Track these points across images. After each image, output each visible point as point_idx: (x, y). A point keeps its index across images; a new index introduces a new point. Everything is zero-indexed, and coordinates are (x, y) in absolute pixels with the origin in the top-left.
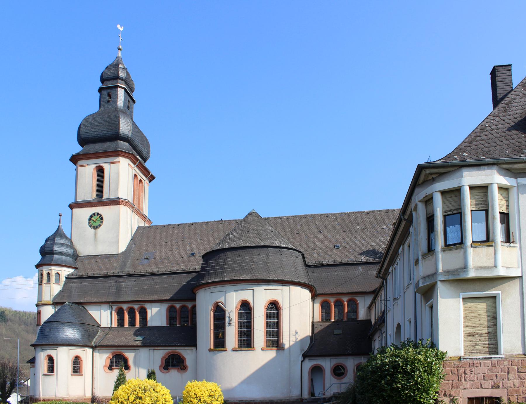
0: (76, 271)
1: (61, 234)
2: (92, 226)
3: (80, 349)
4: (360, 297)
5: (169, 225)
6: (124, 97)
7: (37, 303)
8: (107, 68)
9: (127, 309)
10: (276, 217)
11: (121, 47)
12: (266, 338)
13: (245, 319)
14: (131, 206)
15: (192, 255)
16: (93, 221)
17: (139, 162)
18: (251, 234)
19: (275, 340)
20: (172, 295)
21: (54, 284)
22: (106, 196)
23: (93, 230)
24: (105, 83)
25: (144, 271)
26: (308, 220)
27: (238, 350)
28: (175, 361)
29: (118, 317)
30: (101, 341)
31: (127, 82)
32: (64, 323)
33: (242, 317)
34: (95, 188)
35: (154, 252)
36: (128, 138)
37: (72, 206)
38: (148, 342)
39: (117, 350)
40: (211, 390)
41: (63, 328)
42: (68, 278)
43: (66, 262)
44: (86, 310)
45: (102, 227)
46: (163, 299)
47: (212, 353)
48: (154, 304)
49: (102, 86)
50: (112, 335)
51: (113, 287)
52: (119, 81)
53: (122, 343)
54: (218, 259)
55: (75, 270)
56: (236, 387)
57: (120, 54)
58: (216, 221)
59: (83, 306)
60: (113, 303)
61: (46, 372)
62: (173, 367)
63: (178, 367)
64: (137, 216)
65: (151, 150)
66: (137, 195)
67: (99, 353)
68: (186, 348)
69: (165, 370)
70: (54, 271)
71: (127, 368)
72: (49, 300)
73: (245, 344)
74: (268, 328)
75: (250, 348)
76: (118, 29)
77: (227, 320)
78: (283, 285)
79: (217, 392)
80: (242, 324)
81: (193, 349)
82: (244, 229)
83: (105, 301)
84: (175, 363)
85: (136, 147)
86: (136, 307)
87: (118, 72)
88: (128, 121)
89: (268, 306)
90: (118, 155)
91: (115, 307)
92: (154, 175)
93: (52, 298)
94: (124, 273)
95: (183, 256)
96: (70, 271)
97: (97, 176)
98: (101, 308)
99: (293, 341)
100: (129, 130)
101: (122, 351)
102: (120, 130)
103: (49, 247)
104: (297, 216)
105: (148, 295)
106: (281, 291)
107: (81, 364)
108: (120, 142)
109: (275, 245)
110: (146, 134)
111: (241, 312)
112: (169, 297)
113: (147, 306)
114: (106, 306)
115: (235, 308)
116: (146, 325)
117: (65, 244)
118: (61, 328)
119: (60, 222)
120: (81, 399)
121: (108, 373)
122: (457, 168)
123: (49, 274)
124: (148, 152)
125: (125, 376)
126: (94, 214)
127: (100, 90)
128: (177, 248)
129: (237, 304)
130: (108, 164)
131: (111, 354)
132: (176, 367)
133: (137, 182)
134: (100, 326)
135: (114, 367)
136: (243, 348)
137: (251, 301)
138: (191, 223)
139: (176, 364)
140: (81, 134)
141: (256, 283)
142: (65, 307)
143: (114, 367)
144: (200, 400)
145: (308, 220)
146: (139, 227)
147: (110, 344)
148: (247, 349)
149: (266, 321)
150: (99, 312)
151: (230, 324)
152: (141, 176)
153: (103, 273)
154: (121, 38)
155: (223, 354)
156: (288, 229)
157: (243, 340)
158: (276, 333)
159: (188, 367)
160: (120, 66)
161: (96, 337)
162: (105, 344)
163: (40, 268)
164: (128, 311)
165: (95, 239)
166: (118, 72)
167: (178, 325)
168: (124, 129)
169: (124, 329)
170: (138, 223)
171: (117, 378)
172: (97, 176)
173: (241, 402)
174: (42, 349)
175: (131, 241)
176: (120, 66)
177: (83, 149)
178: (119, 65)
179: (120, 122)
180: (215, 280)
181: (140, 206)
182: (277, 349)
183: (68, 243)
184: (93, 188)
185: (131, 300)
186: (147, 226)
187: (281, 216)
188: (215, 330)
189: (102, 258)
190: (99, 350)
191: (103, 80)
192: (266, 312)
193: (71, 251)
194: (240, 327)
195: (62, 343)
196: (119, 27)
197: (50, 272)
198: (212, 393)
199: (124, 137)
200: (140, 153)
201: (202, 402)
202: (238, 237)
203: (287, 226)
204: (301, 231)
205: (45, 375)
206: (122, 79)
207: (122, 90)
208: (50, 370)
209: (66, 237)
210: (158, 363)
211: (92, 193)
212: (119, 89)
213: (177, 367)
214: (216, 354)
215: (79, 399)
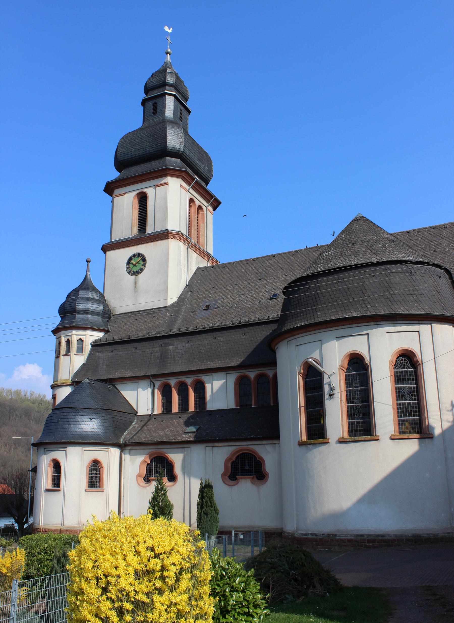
0: (106, 336)
1: (88, 285)
2: (132, 272)
3: (105, 450)
5: (240, 261)
6: (174, 106)
7: (52, 383)
8: (152, 76)
9: (176, 385)
10: (400, 232)
11: (169, 50)
12: (397, 418)
13: (358, 385)
14: (186, 239)
15: (272, 297)
16: (133, 264)
17: (196, 181)
18: (358, 248)
19: (414, 420)
20: (243, 359)
21: (75, 356)
22: (150, 230)
23: (133, 278)
24: (149, 93)
25: (201, 327)
26: (451, 230)
27: (348, 440)
29: (163, 399)
30: (135, 435)
31: (178, 88)
32: (78, 409)
33: (352, 383)
34: (136, 221)
35: (217, 300)
36: (179, 153)
37: (105, 249)
38: (205, 434)
40: (152, 549)
41: (77, 416)
42: (95, 345)
43: (93, 323)
44: (118, 390)
45: (144, 271)
46: (229, 365)
47: (304, 447)
48: (215, 375)
49: (146, 97)
50: (152, 425)
51: (157, 354)
52: (167, 87)
53: (165, 438)
54: (307, 290)
55: (105, 334)
56: (349, 509)
57: (169, 58)
58: (309, 248)
59: (114, 385)
60: (155, 376)
61: (50, 487)
62: (245, 475)
63: (253, 475)
64: (196, 253)
65: (214, 168)
66: (195, 225)
67: (130, 455)
68: (264, 442)
69: (231, 480)
70: (75, 336)
71: (172, 478)
72: (68, 379)
73: (360, 430)
74: (400, 400)
75: (369, 437)
77: (326, 389)
78: (420, 322)
79: (175, 558)
80: (353, 394)
81: (276, 444)
82: (346, 242)
83: (143, 375)
84: (247, 467)
85: (191, 164)
86: (189, 380)
87: (166, 77)
88: (178, 131)
89: (396, 360)
90: (166, 175)
91: (158, 384)
92: (220, 199)
93: (71, 375)
94: (172, 331)
95: (261, 300)
96: (99, 335)
98: (138, 385)
99: (449, 422)
100: (180, 142)
101: (165, 450)
102: (168, 143)
103: (70, 303)
104: (432, 226)
105: (207, 362)
106: (418, 333)
107: (101, 472)
108: (168, 158)
109: (399, 260)
110: (205, 149)
111: (350, 373)
112: (238, 363)
113: (205, 378)
114: (145, 383)
115: (338, 367)
116: (205, 408)
117: (92, 298)
118: (73, 417)
119: (88, 270)
121: (143, 487)
124: (210, 171)
125: (165, 491)
126: (134, 255)
127: (144, 103)
128: (252, 290)
129: (342, 361)
130: (153, 188)
131: (148, 455)
132: (249, 475)
133: (194, 209)
134: (137, 413)
135: (152, 477)
136: (356, 438)
137: (365, 354)
138: (272, 255)
139: (249, 470)
140: (118, 156)
141: (372, 323)
142: (83, 386)
143: (153, 478)
144: (105, 590)
145: (451, 230)
146: (198, 269)
147: (146, 439)
148: (363, 438)
149: (396, 388)
150: (136, 391)
151: (331, 395)
152: (199, 200)
153: (143, 334)
154: (169, 41)
155: (323, 448)
156: (420, 247)
157: (357, 422)
158: (416, 407)
159: (269, 474)
160: (169, 71)
161: (129, 430)
162: (138, 440)
163: (58, 335)
164: (178, 387)
166: (165, 78)
167: (253, 406)
168: (173, 142)
169: (171, 416)
170: (197, 262)
171: (152, 495)
172: (138, 206)
173: (359, 538)
174: (46, 450)
175: (186, 287)
176: (168, 71)
177: (120, 175)
178: (166, 70)
179: (168, 134)
180: (303, 324)
181: (201, 240)
182: (421, 436)
183: (97, 297)
184: (133, 222)
185: (181, 370)
186: (210, 267)
187: (408, 230)
188: (307, 409)
189: (144, 314)
190: (130, 450)
191: (147, 90)
192: (394, 371)
193: (99, 308)
194: (350, 400)
195: (72, 440)
196: (166, 29)
197: (70, 339)
198: (156, 564)
199: (174, 152)
200: (198, 172)
201: (114, 597)
202: (336, 254)
203: (418, 243)
204: (443, 247)
205: (48, 490)
206: (171, 85)
207: (170, 98)
208: (56, 482)
209: (95, 290)
210: (220, 468)
211: (132, 228)
212: (166, 97)
213: (251, 475)
214: (310, 450)
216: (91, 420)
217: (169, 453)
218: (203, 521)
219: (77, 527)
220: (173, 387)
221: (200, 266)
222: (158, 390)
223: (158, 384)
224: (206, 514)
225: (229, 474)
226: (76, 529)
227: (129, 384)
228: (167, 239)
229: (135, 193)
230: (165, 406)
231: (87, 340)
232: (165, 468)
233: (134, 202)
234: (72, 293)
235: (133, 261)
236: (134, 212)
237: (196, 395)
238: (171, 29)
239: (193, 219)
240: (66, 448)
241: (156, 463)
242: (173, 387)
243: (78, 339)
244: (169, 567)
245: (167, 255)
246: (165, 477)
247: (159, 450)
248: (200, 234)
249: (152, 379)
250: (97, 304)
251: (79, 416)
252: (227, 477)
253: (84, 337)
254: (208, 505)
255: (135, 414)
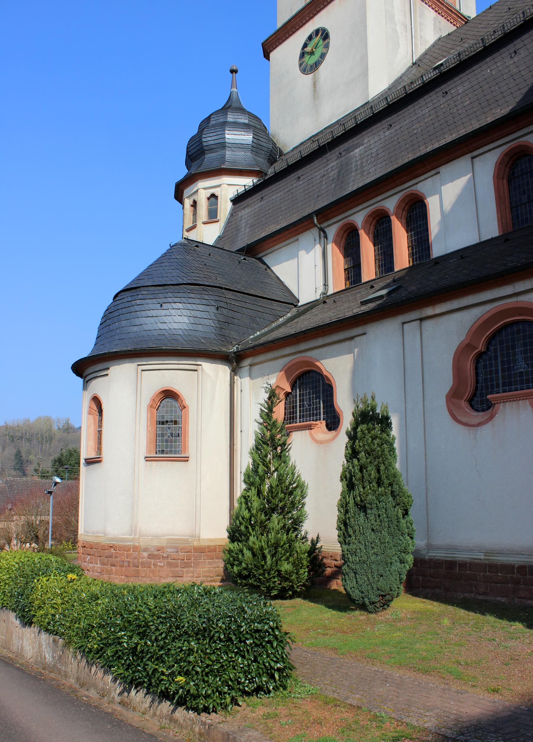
9: (366, 222)
28: (519, 357)
29: (346, 263)
39: (299, 355)
42: (237, 200)
44: (265, 264)
69: (477, 410)
70: (204, 191)
116: (429, 255)
118: (137, 308)
120: (183, 549)
126: (310, 38)
134: (299, 301)
135: (296, 423)
165: (314, 95)
183: (244, 120)
209: (241, 110)
215: (171, 547)
216: (161, 306)
217: (322, 359)
218: (354, 532)
219: (128, 540)
220: (360, 227)
222: (334, 244)
223: (332, 231)
224: (362, 508)
225: (468, 392)
226: (127, 544)
227: (284, 248)
230: (351, 276)
231: (223, 193)
232: (319, 399)
235: (308, 49)
237: (411, 235)
240: (108, 368)
241: (303, 391)
242: (360, 227)
243: (209, 195)
244: (136, 699)
246: (320, 420)
247: (303, 355)
250: (241, 130)
251: (138, 302)
252: (464, 404)
253: (218, 190)
254: (366, 476)
255: (292, 304)
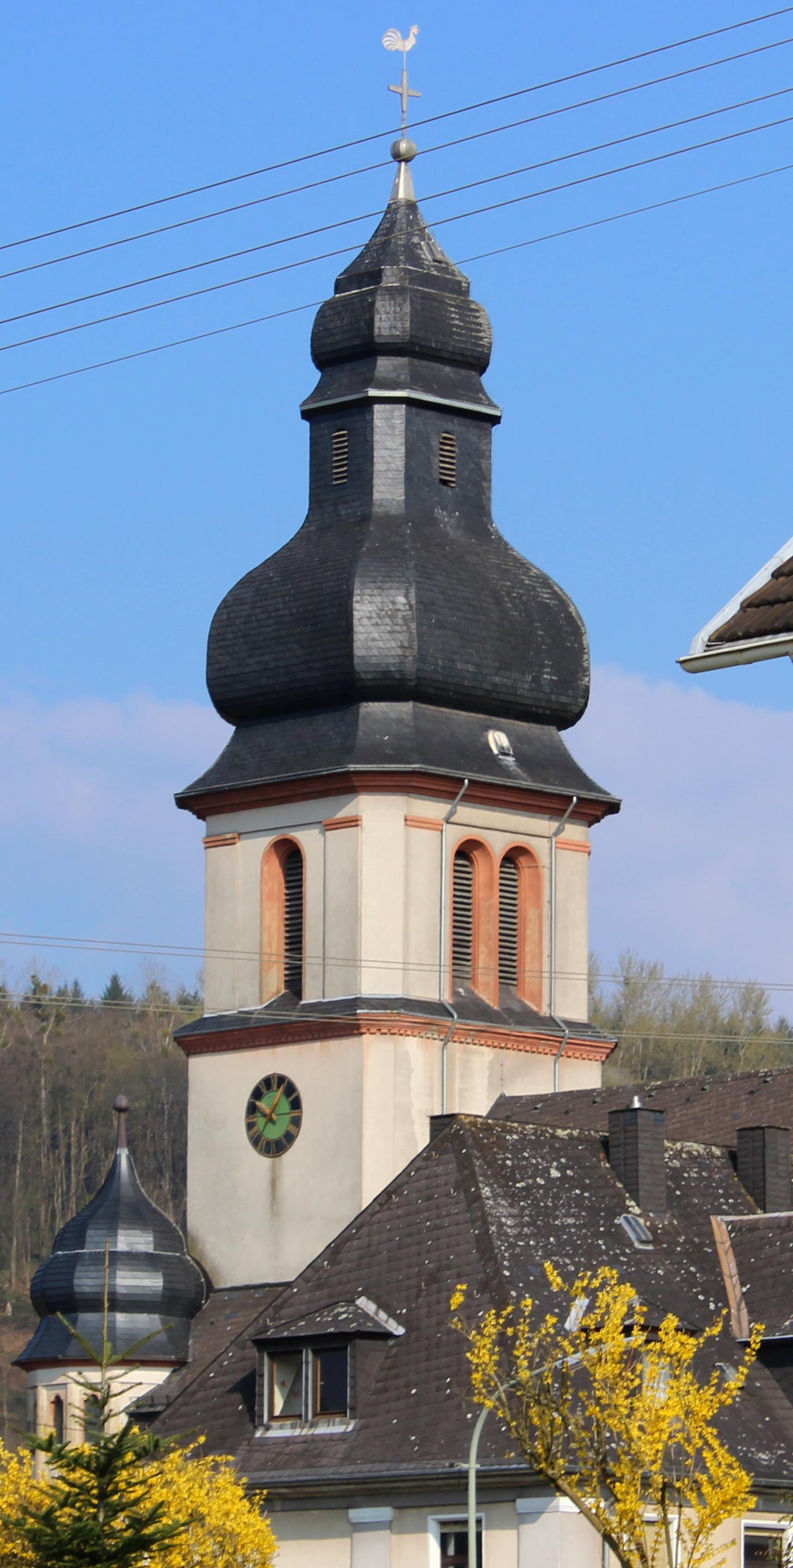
0: (177, 1378)
2: (263, 1142)
4: (339, 1511)
34: (274, 946)
45: (298, 1143)
55: (174, 1372)
66: (490, 938)
76: (390, 51)
96: (153, 1378)
97: (287, 882)
102: (356, 661)
122: (123, 1371)
123: (58, 1403)
130: (317, 831)
172: (284, 885)
197: (63, 1397)
211: (261, 974)
221: (512, 1091)
228: (355, 1034)
229: (266, 841)
233: (266, 875)
234: (66, 1235)
235: (263, 1105)
236: (267, 914)
238: (414, 30)
239: (483, 912)
245: (357, 1093)
248: (527, 949)
249: (568, 1408)
